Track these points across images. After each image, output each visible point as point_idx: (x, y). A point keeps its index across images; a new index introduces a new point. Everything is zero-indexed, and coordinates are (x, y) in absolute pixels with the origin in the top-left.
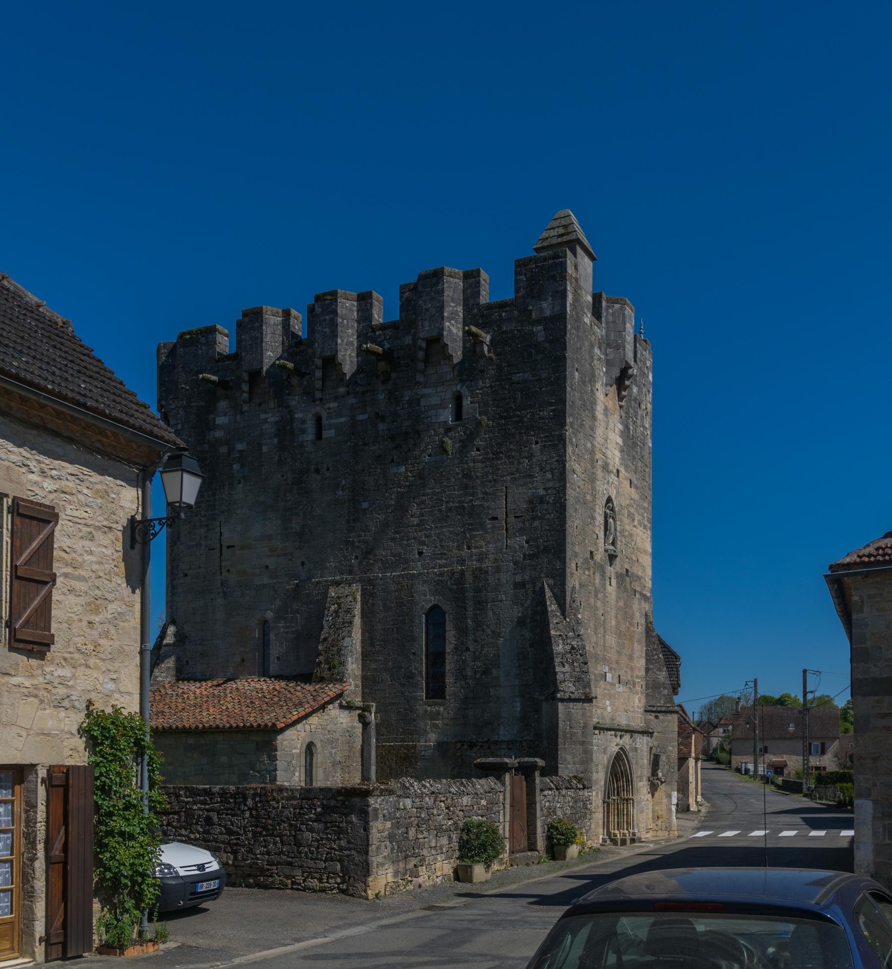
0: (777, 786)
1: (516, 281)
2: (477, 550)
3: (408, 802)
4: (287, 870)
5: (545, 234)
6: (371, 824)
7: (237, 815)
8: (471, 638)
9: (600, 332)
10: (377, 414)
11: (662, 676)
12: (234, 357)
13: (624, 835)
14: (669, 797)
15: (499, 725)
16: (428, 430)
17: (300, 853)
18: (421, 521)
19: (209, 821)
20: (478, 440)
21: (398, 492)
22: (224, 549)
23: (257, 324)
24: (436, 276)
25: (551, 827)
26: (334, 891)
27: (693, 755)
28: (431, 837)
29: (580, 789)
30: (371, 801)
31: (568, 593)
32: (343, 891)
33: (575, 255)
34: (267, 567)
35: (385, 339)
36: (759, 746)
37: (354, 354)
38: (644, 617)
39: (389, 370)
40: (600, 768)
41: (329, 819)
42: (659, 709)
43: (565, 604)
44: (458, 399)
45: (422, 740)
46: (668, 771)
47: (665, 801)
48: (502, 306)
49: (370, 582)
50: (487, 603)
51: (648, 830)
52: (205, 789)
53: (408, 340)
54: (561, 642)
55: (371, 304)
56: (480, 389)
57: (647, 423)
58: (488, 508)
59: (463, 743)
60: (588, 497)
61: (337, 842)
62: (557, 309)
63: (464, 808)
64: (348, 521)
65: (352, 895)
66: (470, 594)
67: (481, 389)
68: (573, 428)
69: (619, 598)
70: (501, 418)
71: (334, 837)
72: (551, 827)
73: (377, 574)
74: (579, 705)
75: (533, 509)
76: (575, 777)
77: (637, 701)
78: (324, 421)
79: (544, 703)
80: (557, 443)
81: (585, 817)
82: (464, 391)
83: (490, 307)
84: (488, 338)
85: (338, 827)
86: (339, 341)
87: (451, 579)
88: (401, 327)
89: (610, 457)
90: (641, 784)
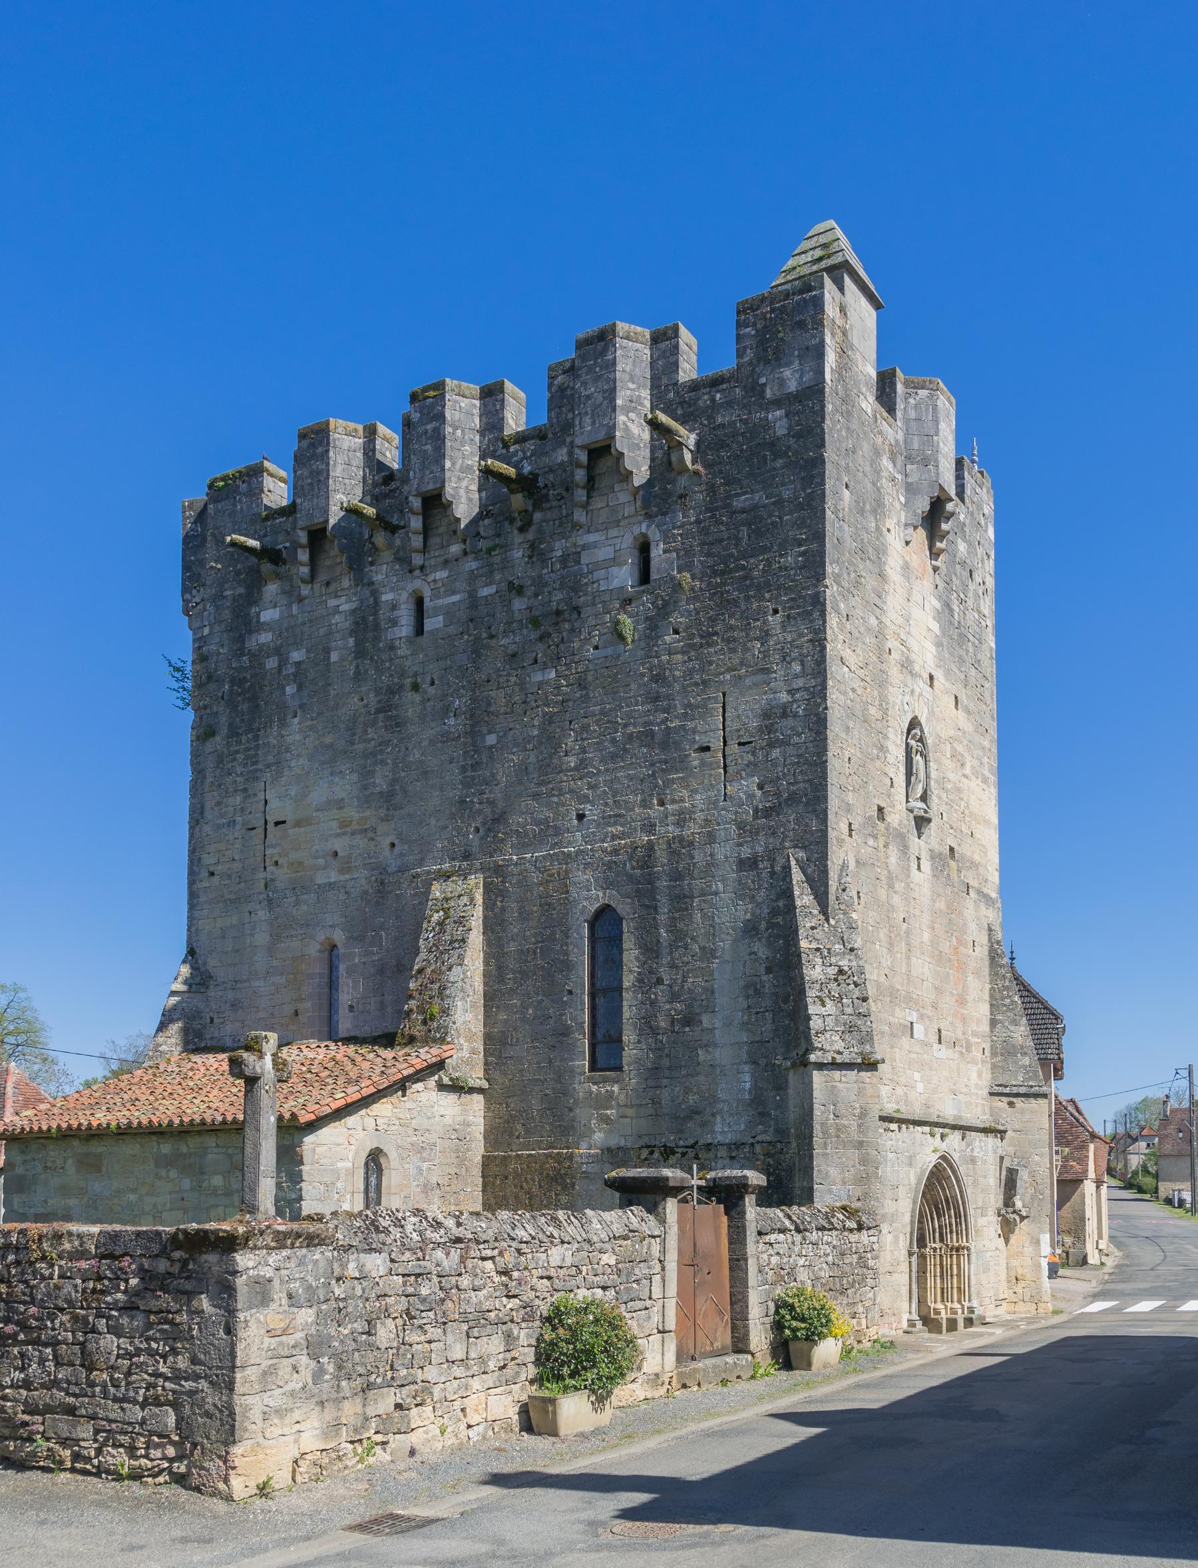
1: (739, 338)
2: (676, 806)
3: (376, 1263)
4: (62, 1424)
5: (791, 263)
6: (241, 1316)
8: (664, 961)
9: (892, 432)
11: (1020, 1033)
12: (290, 511)
14: (1037, 1242)
15: (713, 1115)
17: (92, 1384)
18: (582, 761)
20: (675, 614)
22: (270, 826)
23: (320, 450)
25: (781, 1305)
26: (161, 1479)
27: (1091, 1174)
28: (450, 1338)
29: (851, 1230)
30: (244, 1260)
32: (181, 1480)
33: (841, 289)
34: (336, 854)
35: (525, 458)
37: (474, 487)
39: (530, 509)
40: (902, 1192)
41: (154, 1304)
43: (826, 893)
44: (644, 549)
45: (584, 1145)
46: (1033, 1198)
47: (1029, 1250)
48: (715, 382)
49: (498, 870)
50: (692, 897)
51: (999, 1302)
53: (561, 455)
55: (503, 400)
56: (679, 528)
60: (873, 711)
61: (171, 1359)
62: (808, 377)
63: (552, 1273)
64: (464, 769)
65: (197, 1489)
66: (663, 883)
68: (839, 584)
69: (936, 895)
70: (715, 573)
71: (162, 1347)
72: (781, 1305)
74: (852, 1075)
75: (770, 729)
76: (844, 1208)
77: (974, 1076)
78: (427, 603)
79: (791, 1073)
80: (813, 608)
82: (654, 534)
83: (694, 386)
84: (691, 439)
85: (171, 1322)
86: (448, 464)
87: (631, 858)
88: (550, 436)
89: (915, 649)
90: (982, 1221)
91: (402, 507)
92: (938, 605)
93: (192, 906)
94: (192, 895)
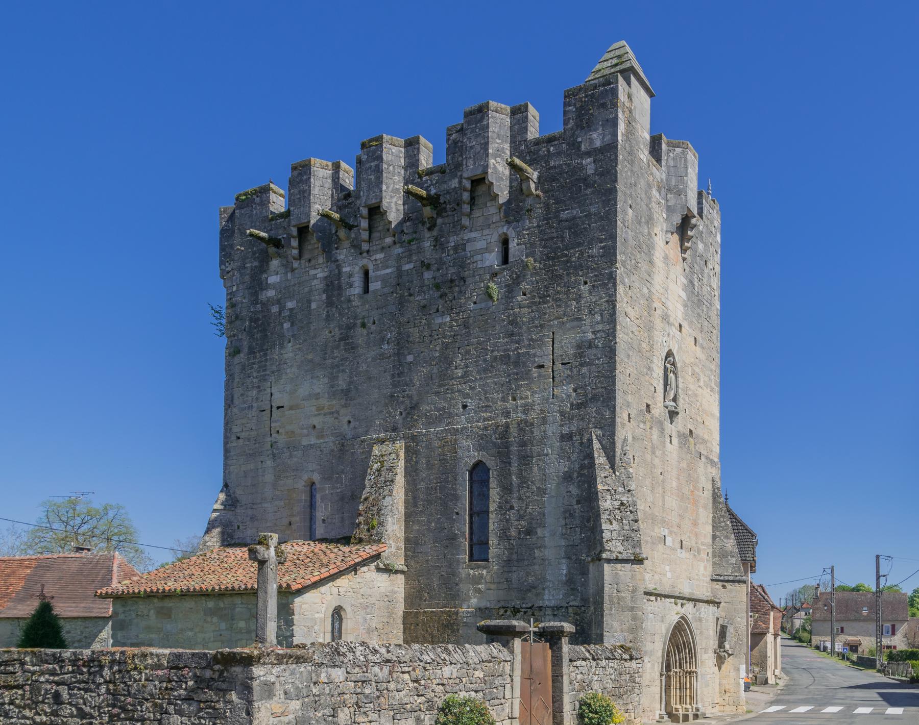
0: (852, 662)
1: (565, 113)
2: (523, 401)
3: (338, 674)
5: (598, 67)
6: (256, 704)
7: (91, 691)
8: (515, 496)
9: (659, 174)
10: (422, 262)
11: (730, 544)
12: (286, 215)
13: (687, 710)
14: (738, 670)
15: (544, 589)
16: (474, 276)
18: (466, 372)
19: (57, 696)
21: (443, 343)
22: (274, 409)
24: (482, 111)
25: (583, 703)
27: (771, 630)
29: (626, 660)
30: (257, 671)
31: (618, 445)
33: (629, 84)
34: (314, 427)
35: (432, 184)
36: (837, 626)
37: (401, 202)
38: (710, 482)
39: (435, 216)
41: (203, 697)
42: (726, 578)
43: (614, 456)
44: (505, 242)
45: (465, 606)
47: (733, 674)
48: (550, 140)
49: (414, 438)
50: (532, 457)
51: (714, 705)
52: (54, 655)
53: (454, 183)
54: (609, 497)
55: (418, 149)
56: (527, 230)
57: (716, 283)
58: (535, 355)
59: (505, 609)
60: (644, 345)
62: (608, 138)
63: (445, 681)
67: (529, 229)
68: (625, 267)
70: (549, 258)
72: (583, 703)
73: (420, 430)
74: (628, 566)
75: (581, 355)
76: (622, 646)
77: (702, 569)
78: (371, 274)
79: (591, 565)
81: (632, 691)
82: (511, 233)
83: (537, 142)
84: (534, 175)
85: (214, 708)
86: (384, 188)
87: (495, 433)
88: (448, 171)
89: (671, 308)
90: (705, 656)
91: (356, 214)
92: (685, 282)
93: (226, 458)
94: (226, 451)
